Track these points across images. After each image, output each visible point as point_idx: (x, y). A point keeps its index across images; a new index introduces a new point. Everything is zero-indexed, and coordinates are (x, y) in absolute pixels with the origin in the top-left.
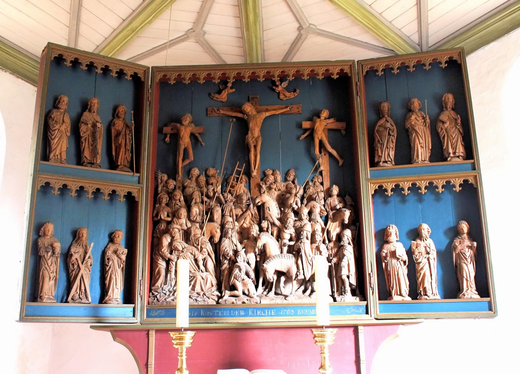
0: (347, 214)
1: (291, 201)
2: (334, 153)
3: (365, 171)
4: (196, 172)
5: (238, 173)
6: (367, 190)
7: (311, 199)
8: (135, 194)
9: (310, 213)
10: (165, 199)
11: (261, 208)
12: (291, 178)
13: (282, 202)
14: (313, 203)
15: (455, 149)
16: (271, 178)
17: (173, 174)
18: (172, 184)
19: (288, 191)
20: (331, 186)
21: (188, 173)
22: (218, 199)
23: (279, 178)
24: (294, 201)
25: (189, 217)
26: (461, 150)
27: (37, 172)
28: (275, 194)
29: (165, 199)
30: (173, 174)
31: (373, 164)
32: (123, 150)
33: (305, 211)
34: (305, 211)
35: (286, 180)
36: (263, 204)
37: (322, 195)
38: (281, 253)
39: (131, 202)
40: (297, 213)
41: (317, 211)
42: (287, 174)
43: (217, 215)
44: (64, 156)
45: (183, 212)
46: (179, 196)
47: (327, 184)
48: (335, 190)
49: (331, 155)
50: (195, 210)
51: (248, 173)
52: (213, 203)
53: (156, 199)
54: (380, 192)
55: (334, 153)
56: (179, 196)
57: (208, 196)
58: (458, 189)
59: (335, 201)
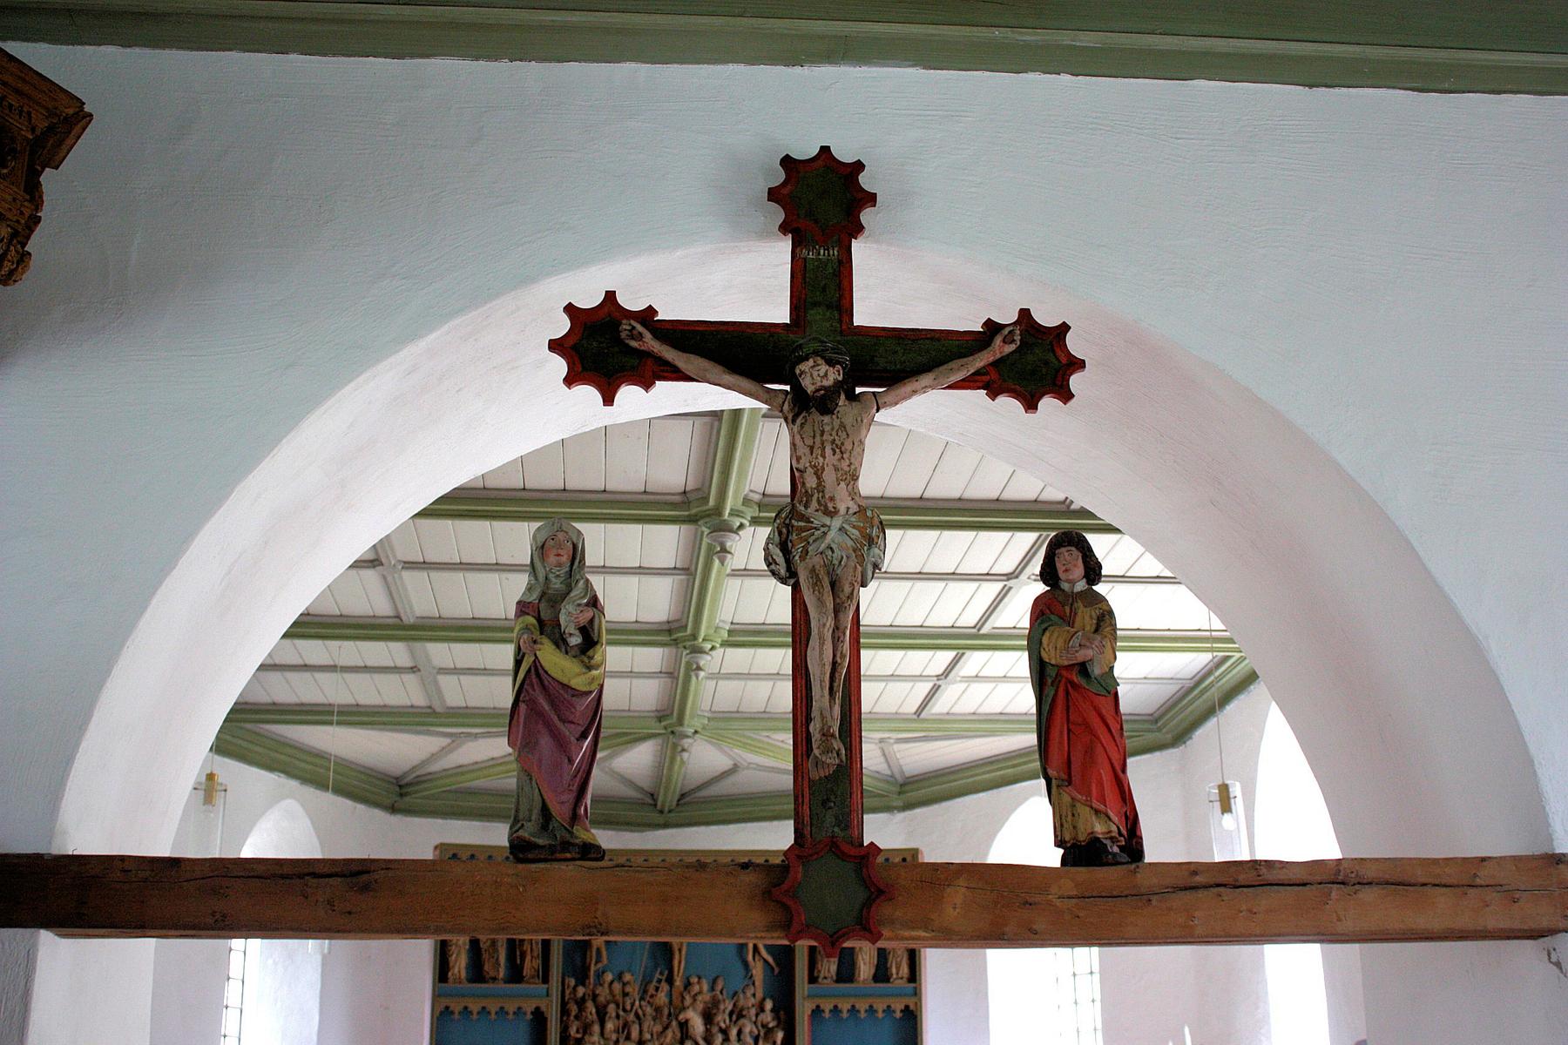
0: (780, 1035)
1: (719, 1018)
2: (770, 959)
3: (802, 986)
4: (609, 977)
5: (659, 981)
6: (803, 1009)
7: (741, 1016)
8: (543, 1009)
9: (740, 1033)
10: (574, 1009)
11: (684, 1026)
12: (719, 987)
13: (708, 1017)
14: (742, 1021)
15: (898, 969)
16: (696, 988)
17: (582, 979)
18: (581, 991)
19: (715, 1003)
20: (764, 999)
21: (600, 975)
22: (637, 1014)
23: (705, 987)
24: (722, 1019)
25: (602, 1034)
26: (905, 970)
27: (436, 996)
28: (700, 1006)
29: (574, 1009)
30: (582, 979)
31: (813, 979)
32: (528, 958)
33: (734, 1032)
34: (734, 1032)
35: (712, 989)
36: (687, 1021)
37: (753, 1011)
38: (1096, 631)
39: (539, 1018)
40: (725, 1032)
41: (747, 1030)
42: (714, 981)
43: (635, 1034)
44: (463, 974)
45: (596, 1028)
46: (591, 1007)
47: (760, 995)
48: (769, 1005)
49: (765, 961)
50: (610, 1026)
51: (670, 981)
52: (632, 1017)
53: (564, 1011)
54: (817, 1011)
55: (770, 959)
56: (591, 1007)
57: (624, 1010)
58: (898, 1015)
59: (767, 1017)
